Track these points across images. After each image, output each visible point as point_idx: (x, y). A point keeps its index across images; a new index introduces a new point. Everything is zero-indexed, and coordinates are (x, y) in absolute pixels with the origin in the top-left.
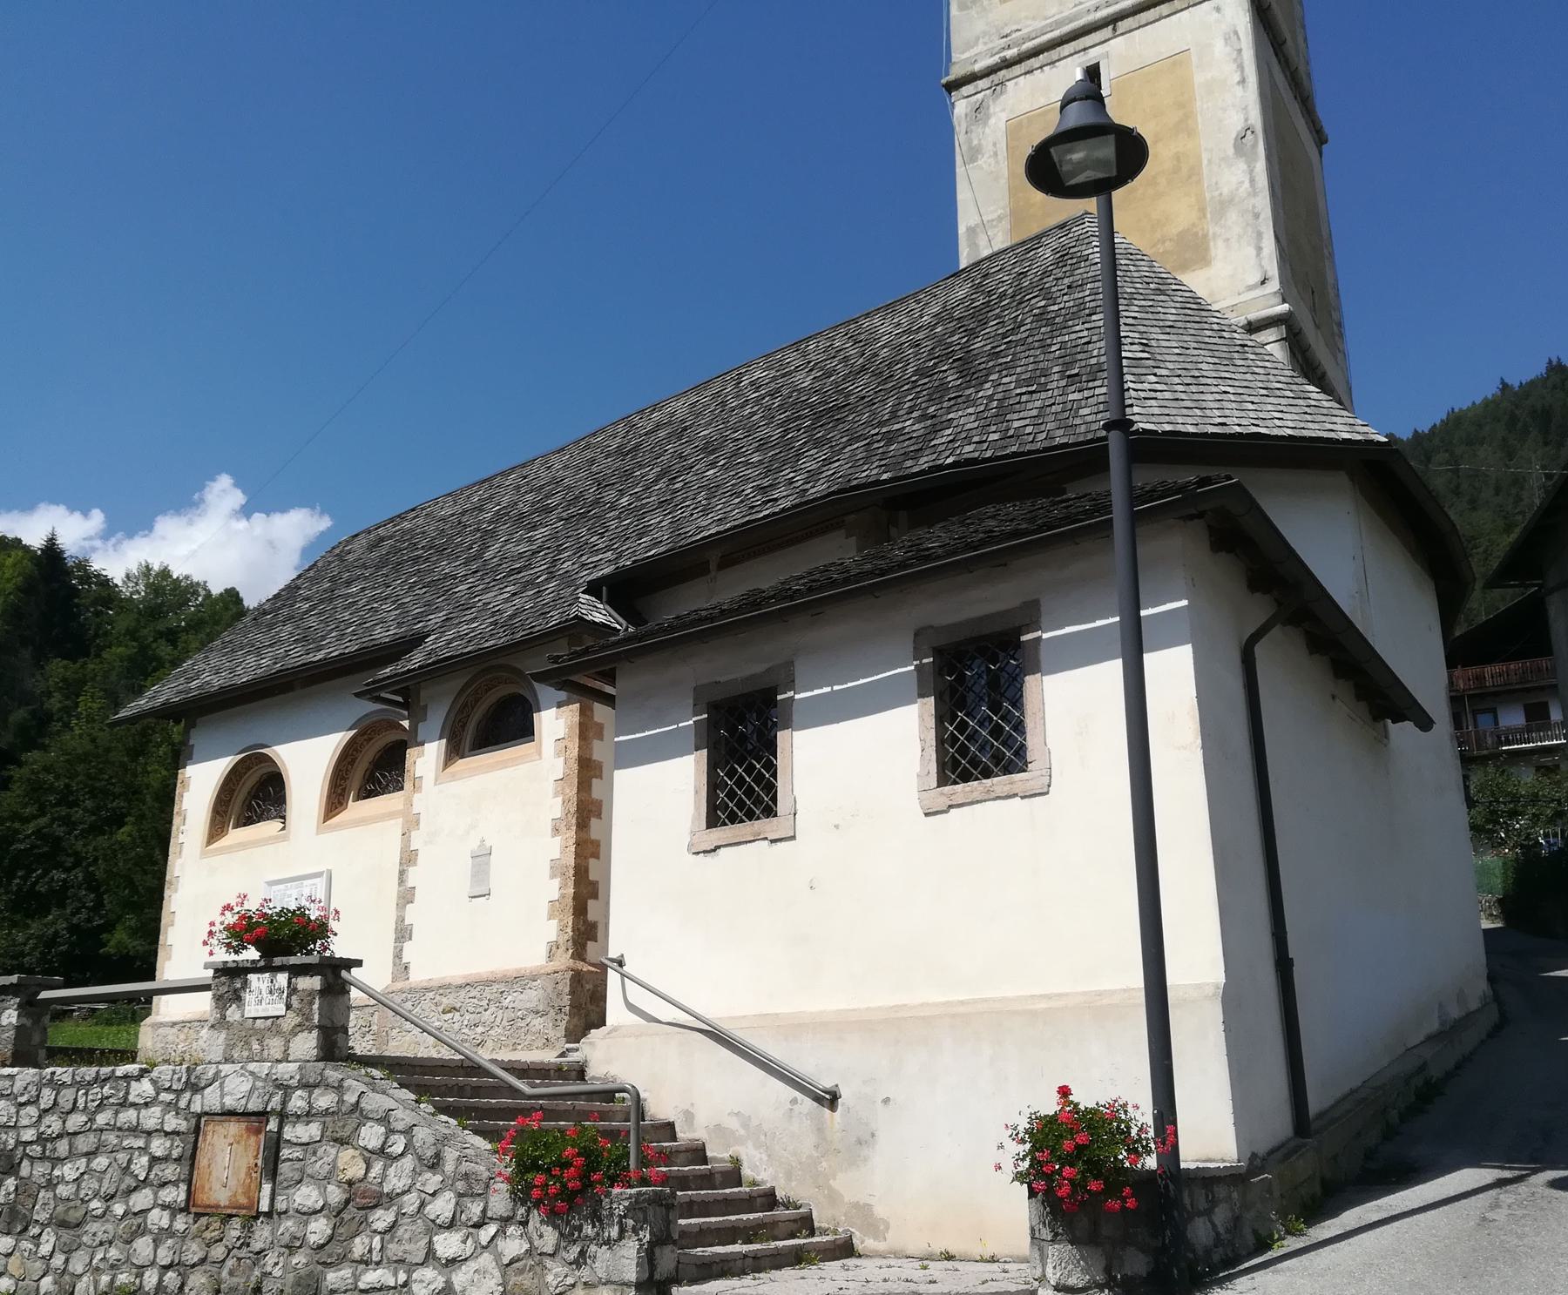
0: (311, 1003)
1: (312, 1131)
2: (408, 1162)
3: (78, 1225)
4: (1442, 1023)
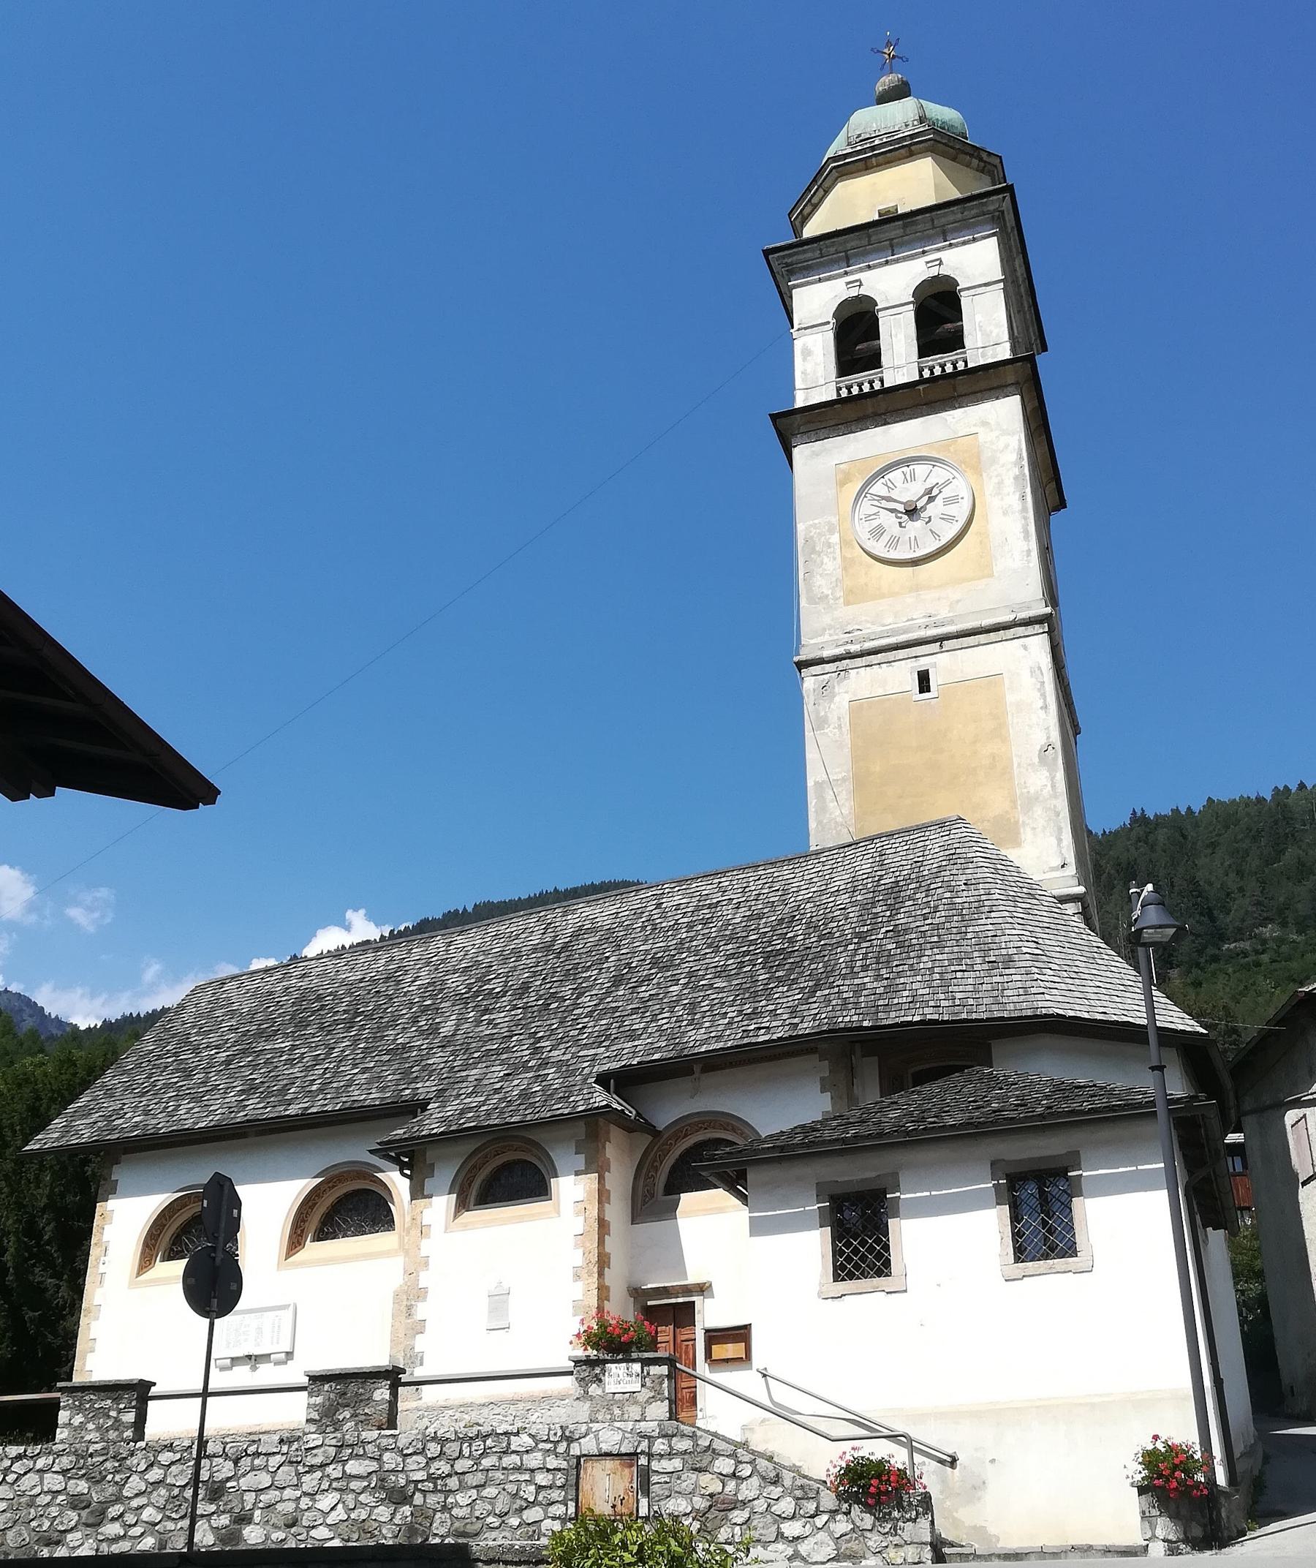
0: (661, 1383)
1: (677, 1463)
2: (755, 1481)
3: (476, 1535)
4: (1245, 1447)
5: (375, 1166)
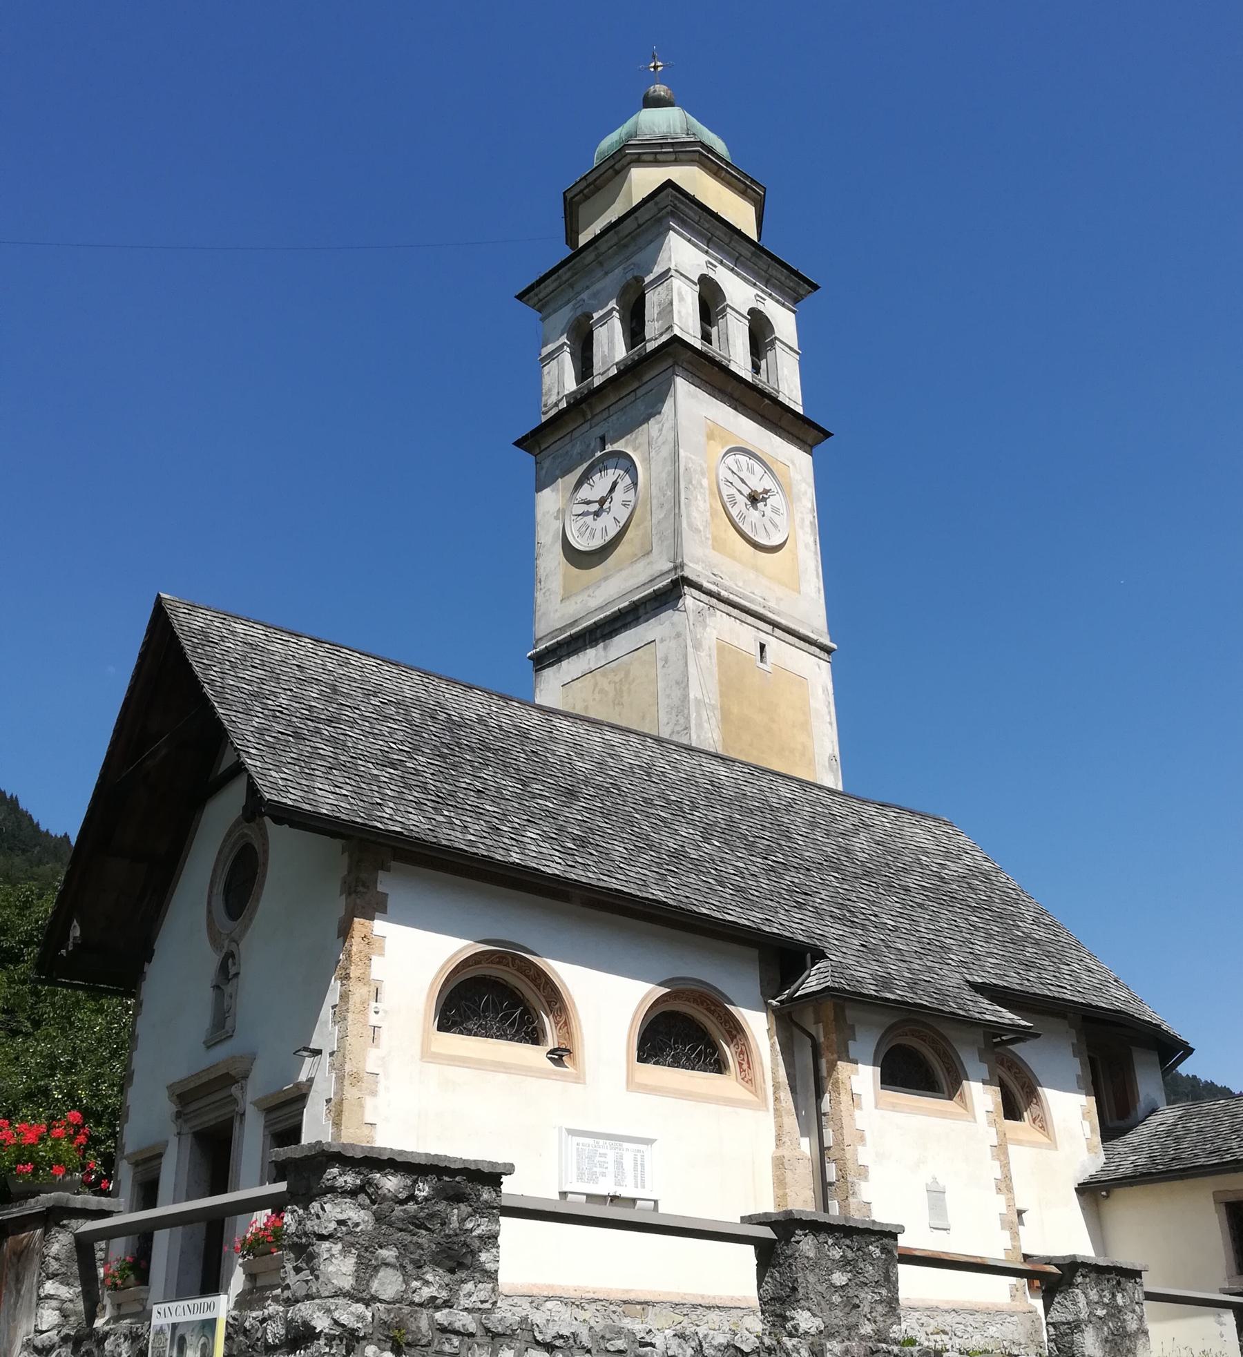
5: (726, 996)
